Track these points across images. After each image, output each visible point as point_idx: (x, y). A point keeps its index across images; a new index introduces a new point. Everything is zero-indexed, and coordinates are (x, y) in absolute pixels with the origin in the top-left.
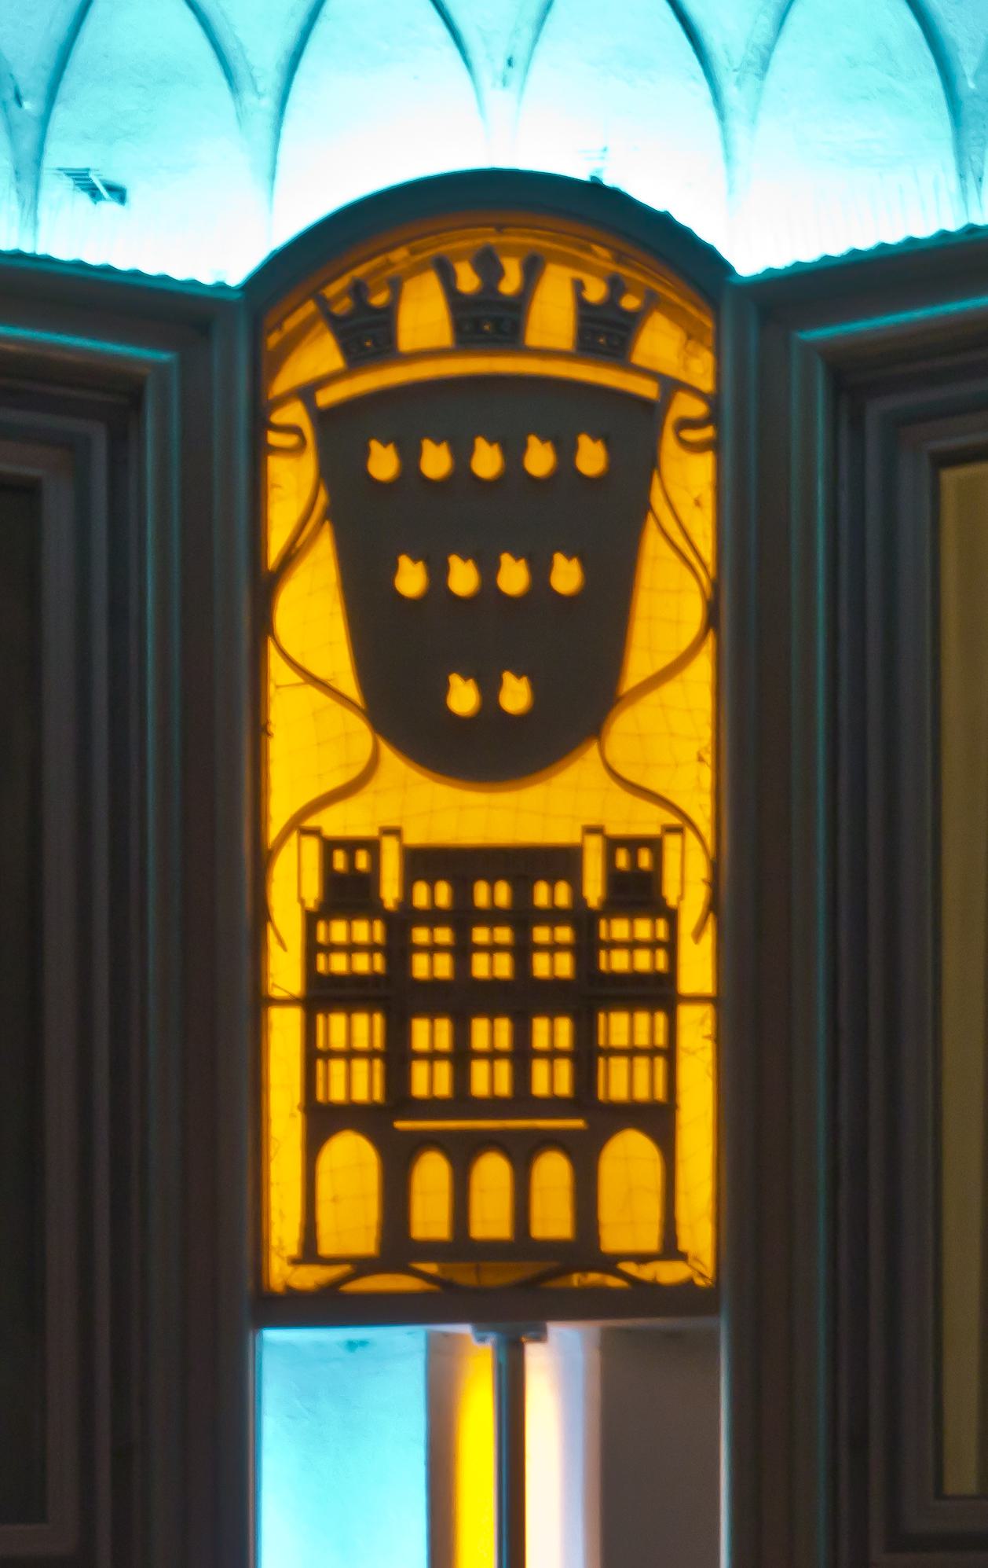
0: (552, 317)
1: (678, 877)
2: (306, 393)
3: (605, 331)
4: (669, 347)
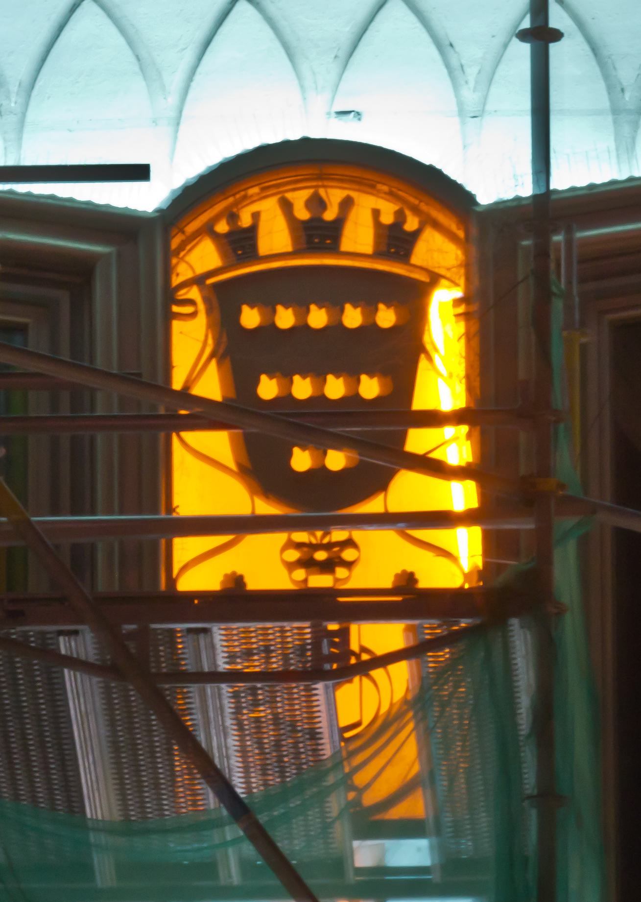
0: (358, 237)
1: (402, 740)
2: (199, 280)
3: (396, 241)
4: (438, 250)
